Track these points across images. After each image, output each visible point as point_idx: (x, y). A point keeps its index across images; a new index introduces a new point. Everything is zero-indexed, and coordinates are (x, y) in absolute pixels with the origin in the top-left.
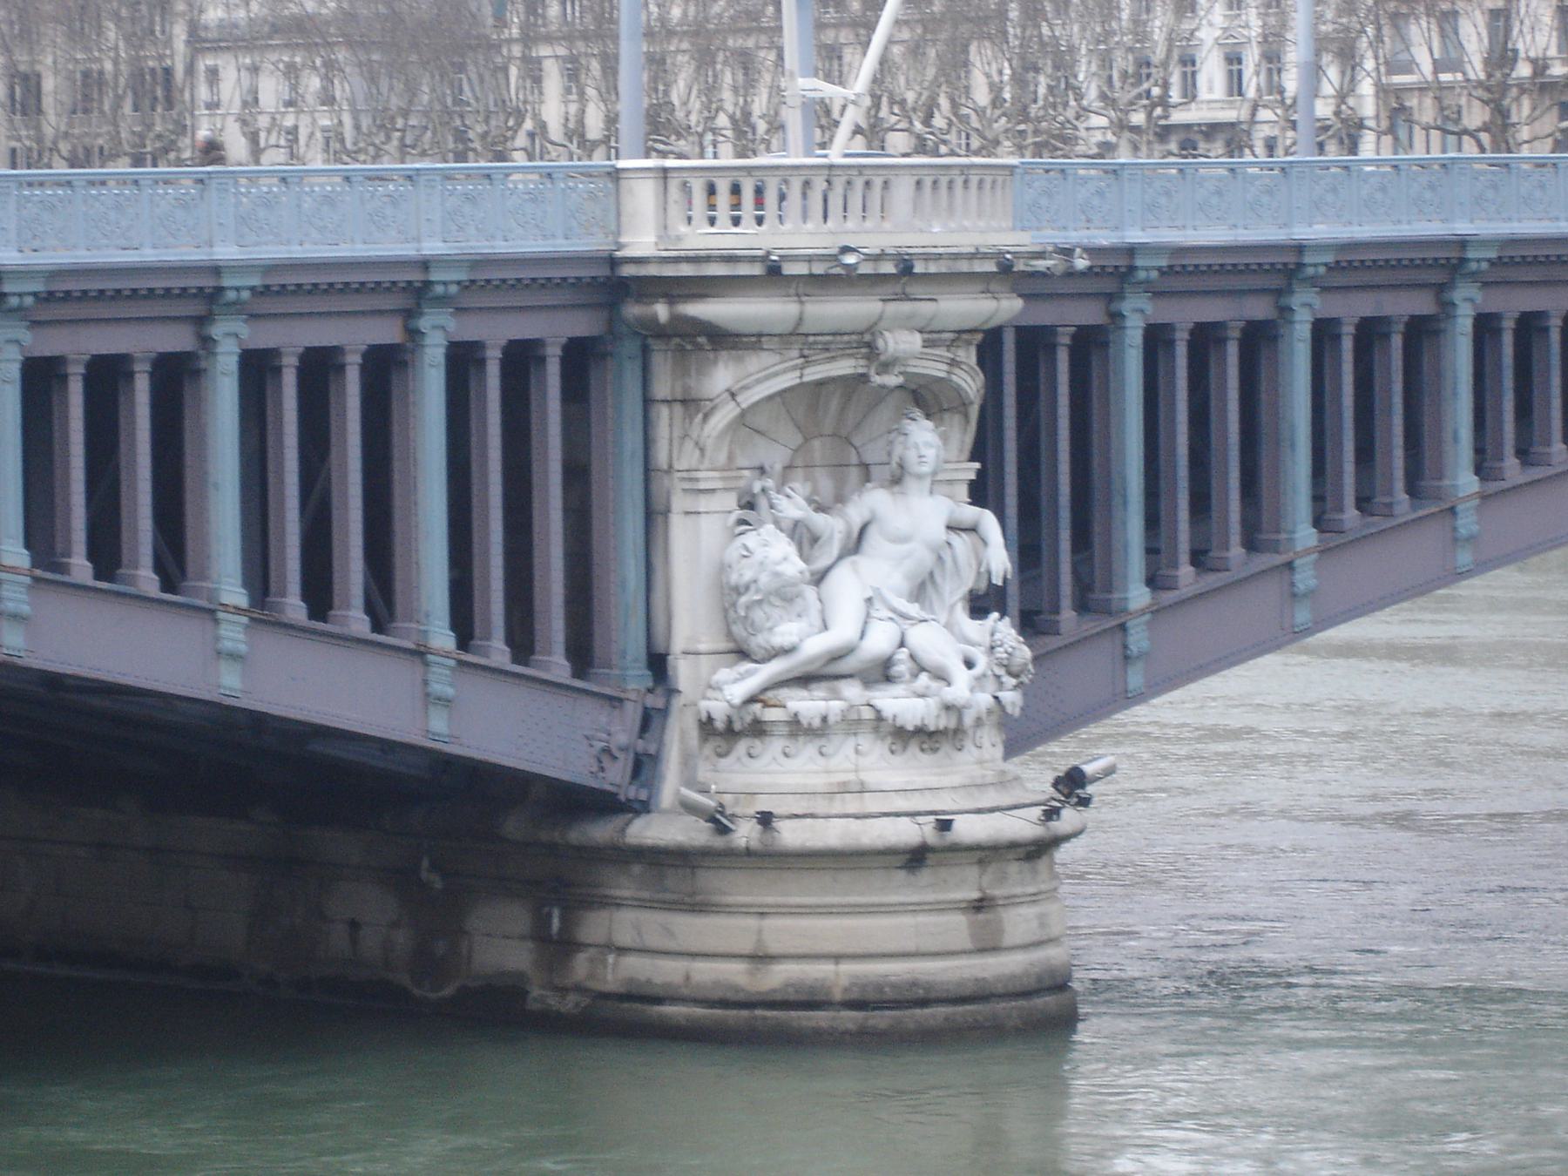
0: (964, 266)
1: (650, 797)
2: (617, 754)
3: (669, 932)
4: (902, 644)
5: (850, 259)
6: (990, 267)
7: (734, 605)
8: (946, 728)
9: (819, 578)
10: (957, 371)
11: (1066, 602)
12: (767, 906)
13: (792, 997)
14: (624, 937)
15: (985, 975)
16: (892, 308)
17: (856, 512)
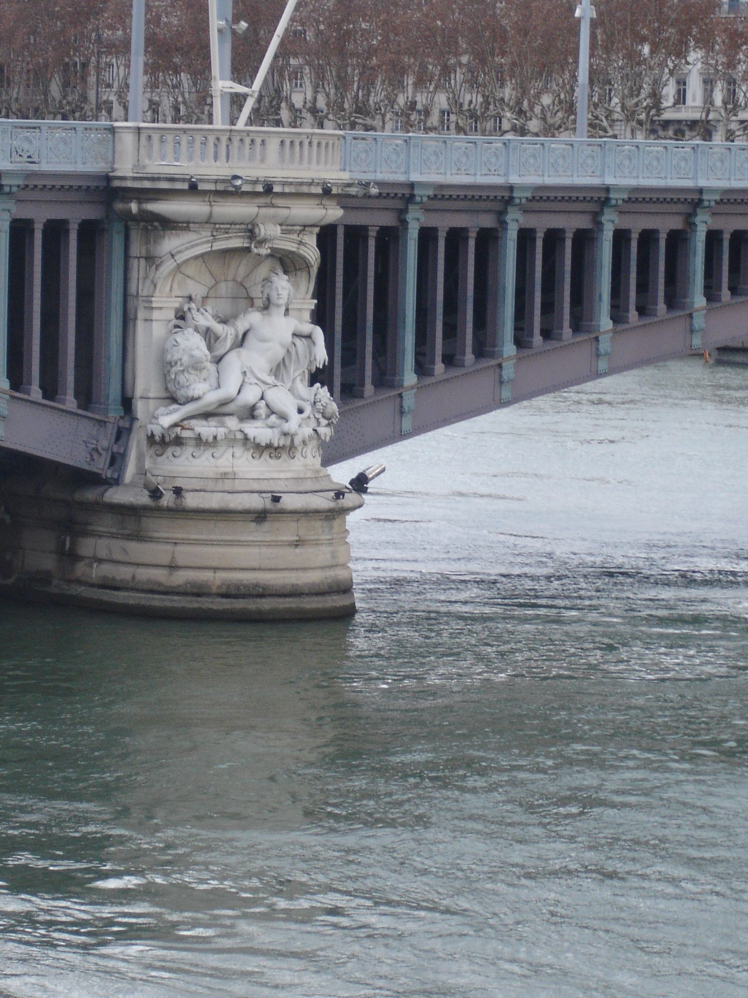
0: (305, 189)
1: (119, 475)
2: (101, 451)
3: (125, 551)
4: (262, 398)
5: (238, 182)
6: (319, 190)
7: (169, 372)
8: (284, 446)
9: (218, 360)
10: (302, 247)
11: (368, 380)
12: (178, 539)
13: (189, 590)
14: (102, 553)
15: (299, 582)
16: (263, 211)
17: (242, 325)
